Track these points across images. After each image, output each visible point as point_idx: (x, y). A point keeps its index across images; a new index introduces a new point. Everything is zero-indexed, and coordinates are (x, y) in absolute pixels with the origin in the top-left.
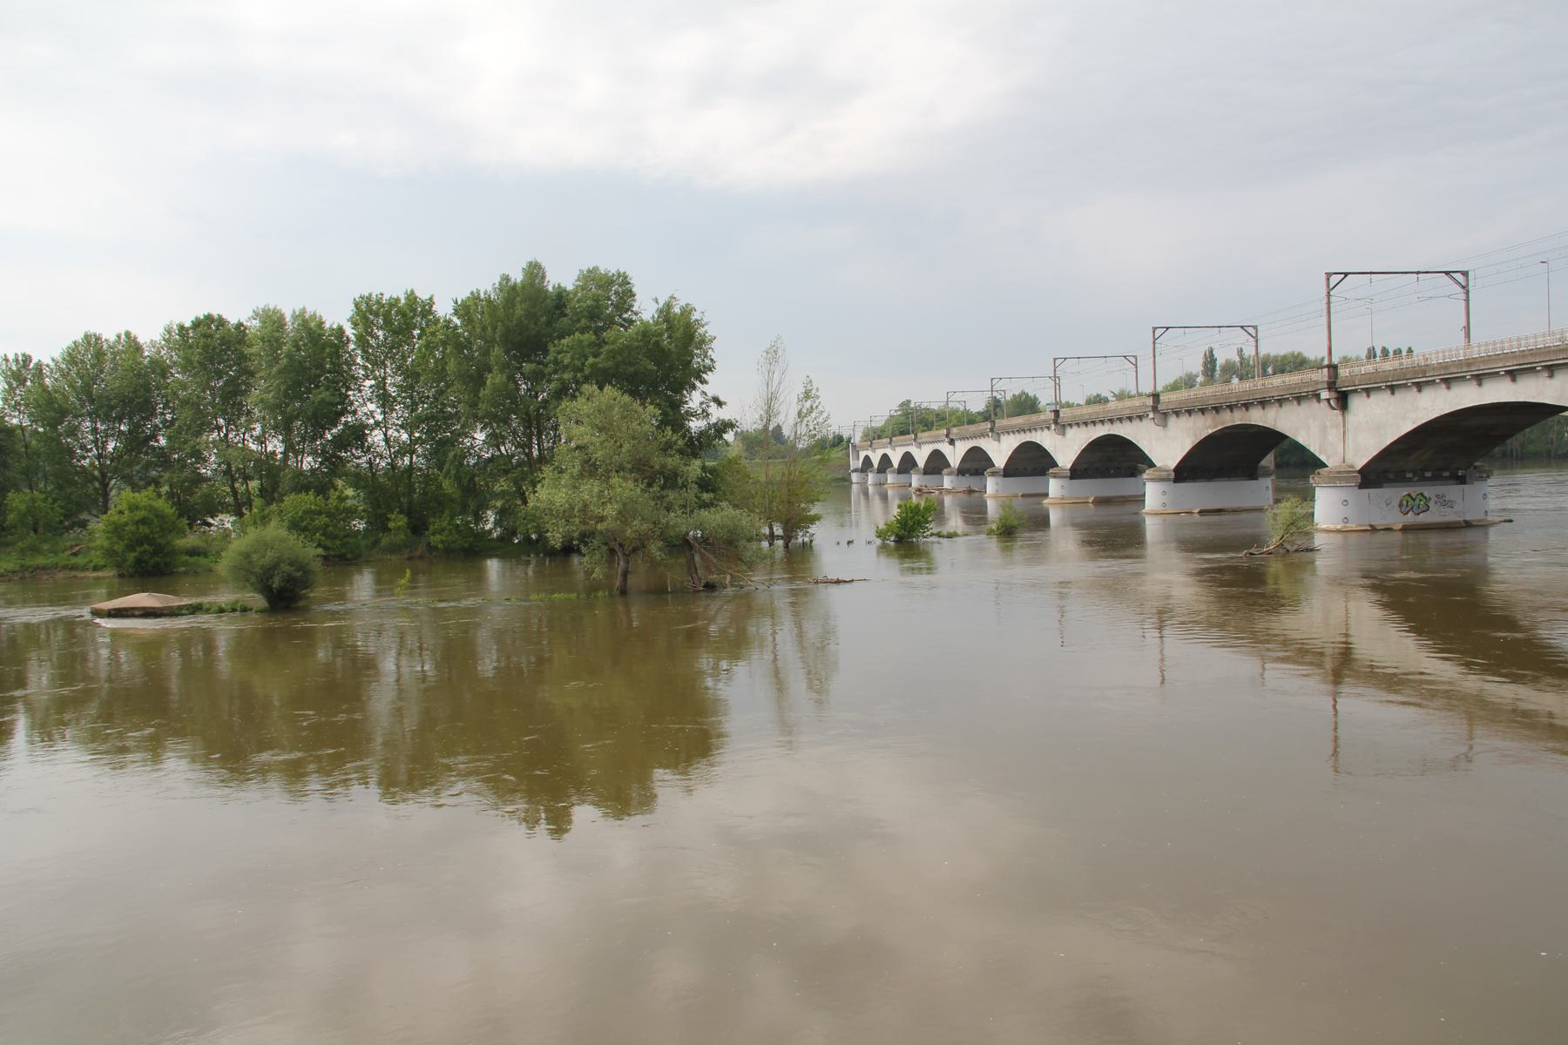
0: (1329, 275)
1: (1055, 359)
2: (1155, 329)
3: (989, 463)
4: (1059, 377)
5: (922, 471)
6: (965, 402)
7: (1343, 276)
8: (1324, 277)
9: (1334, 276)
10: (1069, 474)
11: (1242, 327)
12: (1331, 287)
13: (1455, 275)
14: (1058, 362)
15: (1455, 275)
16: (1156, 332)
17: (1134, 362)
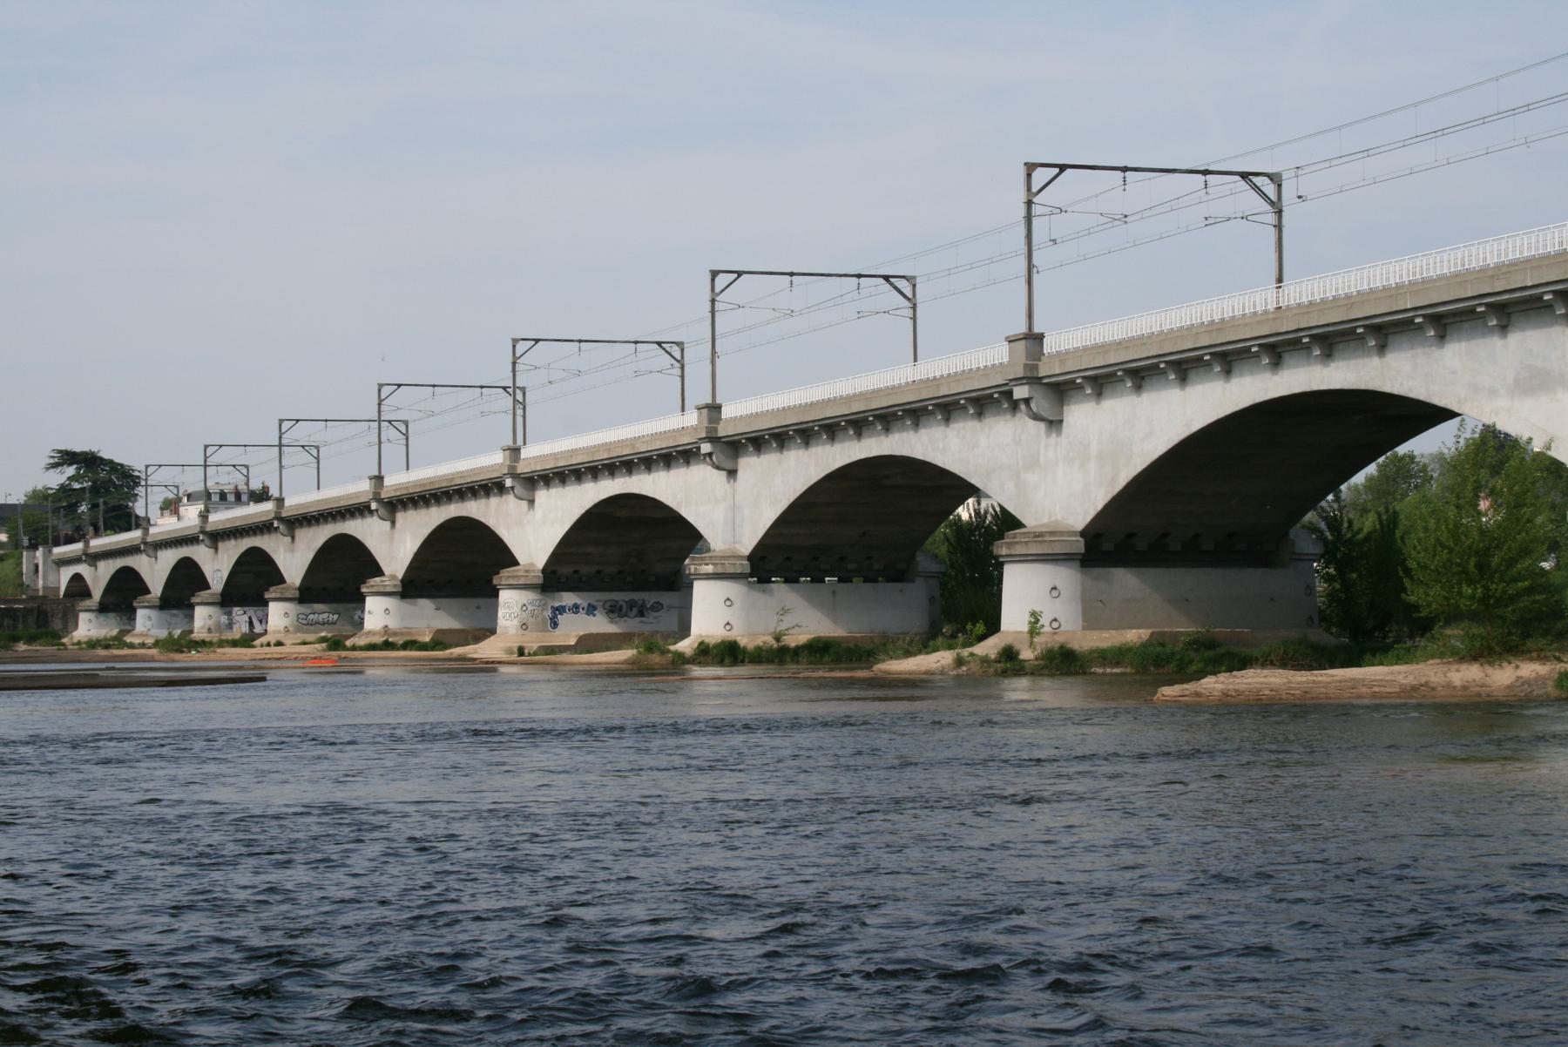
0: (1031, 168)
1: (714, 274)
2: (380, 386)
3: (505, 557)
4: (523, 390)
5: (296, 593)
6: (317, 448)
7: (1057, 170)
8: (1021, 173)
9: (521, 342)
10: (400, 589)
11: (887, 278)
12: (1035, 189)
13: (1257, 180)
14: (386, 391)
15: (1257, 180)
16: (717, 279)
17: (1272, 195)
